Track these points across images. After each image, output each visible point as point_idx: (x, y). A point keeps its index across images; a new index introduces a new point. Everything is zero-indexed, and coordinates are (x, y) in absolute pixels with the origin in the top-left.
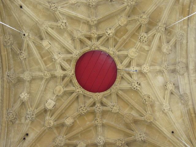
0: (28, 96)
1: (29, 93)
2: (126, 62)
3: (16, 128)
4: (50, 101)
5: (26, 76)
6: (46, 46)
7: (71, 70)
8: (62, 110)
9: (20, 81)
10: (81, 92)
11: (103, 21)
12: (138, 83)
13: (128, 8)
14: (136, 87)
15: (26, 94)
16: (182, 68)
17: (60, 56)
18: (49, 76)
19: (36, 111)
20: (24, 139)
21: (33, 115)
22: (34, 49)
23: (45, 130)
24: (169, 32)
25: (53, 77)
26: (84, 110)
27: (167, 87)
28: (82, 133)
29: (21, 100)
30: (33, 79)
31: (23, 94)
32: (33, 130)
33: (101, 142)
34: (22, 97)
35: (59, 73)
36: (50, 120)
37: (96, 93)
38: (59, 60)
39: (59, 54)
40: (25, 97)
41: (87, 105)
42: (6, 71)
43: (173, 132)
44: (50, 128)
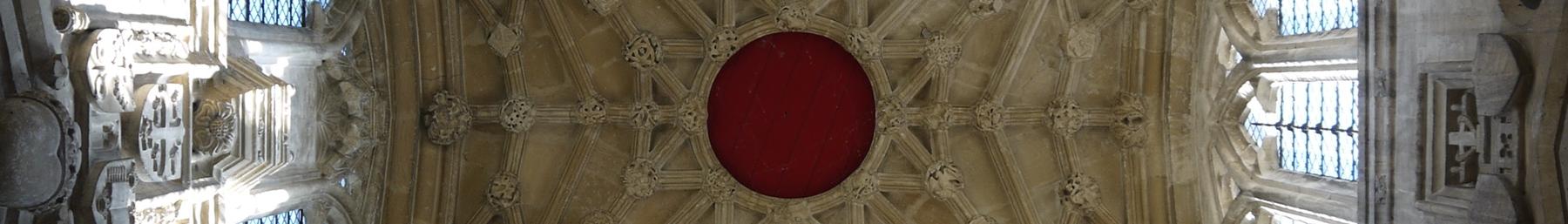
10: (714, 52)
26: (645, 57)
33: (514, 115)
37: (704, 111)
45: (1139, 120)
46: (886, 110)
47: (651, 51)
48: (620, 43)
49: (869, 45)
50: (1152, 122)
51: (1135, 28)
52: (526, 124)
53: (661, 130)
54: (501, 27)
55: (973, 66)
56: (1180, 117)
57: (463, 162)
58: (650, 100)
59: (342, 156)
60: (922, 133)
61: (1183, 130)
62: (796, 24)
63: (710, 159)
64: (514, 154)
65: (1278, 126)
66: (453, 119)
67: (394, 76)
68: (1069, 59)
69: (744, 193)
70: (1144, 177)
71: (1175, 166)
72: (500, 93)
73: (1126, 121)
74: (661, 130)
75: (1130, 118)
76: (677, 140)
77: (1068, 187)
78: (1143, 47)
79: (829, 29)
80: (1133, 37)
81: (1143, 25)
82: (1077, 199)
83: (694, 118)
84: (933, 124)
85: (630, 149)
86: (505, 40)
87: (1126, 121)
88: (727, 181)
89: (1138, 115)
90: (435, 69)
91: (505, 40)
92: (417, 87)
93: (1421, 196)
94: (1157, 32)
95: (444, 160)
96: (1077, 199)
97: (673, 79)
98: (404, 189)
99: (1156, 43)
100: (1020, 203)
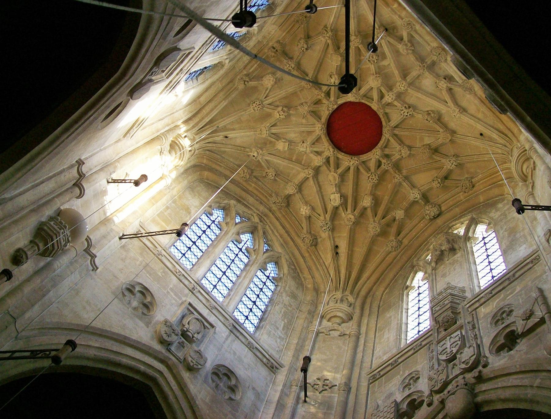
0: (309, 208)
1: (306, 203)
2: (375, 96)
3: (322, 248)
4: (332, 197)
5: (290, 190)
6: (284, 148)
7: (327, 149)
8: (353, 195)
9: (288, 199)
10: (357, 162)
11: (318, 73)
12: (407, 107)
13: (329, 41)
14: (408, 113)
15: (305, 208)
16: (439, 54)
17: (305, 145)
18: (311, 172)
19: (328, 216)
20: (337, 253)
21: (327, 224)
22: (275, 160)
23: (351, 229)
24: (393, 30)
25: (317, 171)
26: (373, 177)
27: (440, 87)
28: (391, 201)
29: (306, 217)
30: (300, 188)
31: (302, 210)
32: (424, 69)
33: (416, 196)
34: (304, 213)
35: (317, 161)
36: (347, 217)
37: (373, 151)
38: (308, 149)
39: (303, 142)
40: (307, 211)
41: (373, 170)
42: (268, 200)
43: (481, 134)
44: (354, 223)
45: (274, 48)
46: (330, 109)
47: (370, 177)
48: (376, 186)
49: (319, 129)
50: (271, 44)
51: (253, 72)
52: (416, 191)
53: (387, 156)
54: (397, 218)
55: (301, 97)
56: (262, 41)
57: (440, 197)
58: (383, 166)
59: (453, 246)
60: (328, 94)
61: (264, 37)
62: (331, 150)
63: (383, 139)
64: (426, 187)
65: (214, 221)
66: (431, 211)
67: (430, 236)
68: (276, 79)
69: (384, 123)
70: (285, 33)
71: (274, 31)
72: (415, 202)
73: (277, 51)
74: (387, 156)
75: (275, 50)
76: (387, 151)
77: (305, 50)
78: (256, 65)
79: (325, 140)
80: (256, 69)
81: (251, 71)
82: (305, 46)
83: (374, 156)
84: (323, 95)
85: (400, 160)
86: (399, 214)
87: (277, 51)
88: (385, 130)
89: (273, 50)
90: (421, 225)
91: (399, 214)
92: (430, 225)
93: (190, 304)
94: (249, 67)
95: (443, 203)
96: (305, 46)
97: (372, 165)
98: (457, 209)
99: (251, 65)
100: (320, 57)
